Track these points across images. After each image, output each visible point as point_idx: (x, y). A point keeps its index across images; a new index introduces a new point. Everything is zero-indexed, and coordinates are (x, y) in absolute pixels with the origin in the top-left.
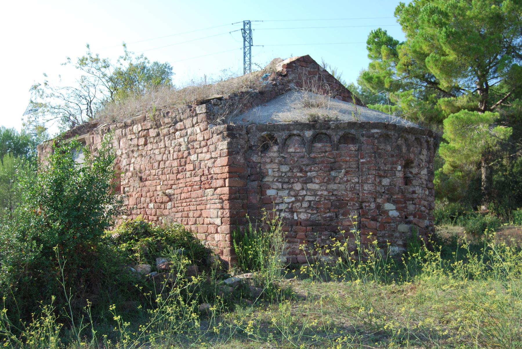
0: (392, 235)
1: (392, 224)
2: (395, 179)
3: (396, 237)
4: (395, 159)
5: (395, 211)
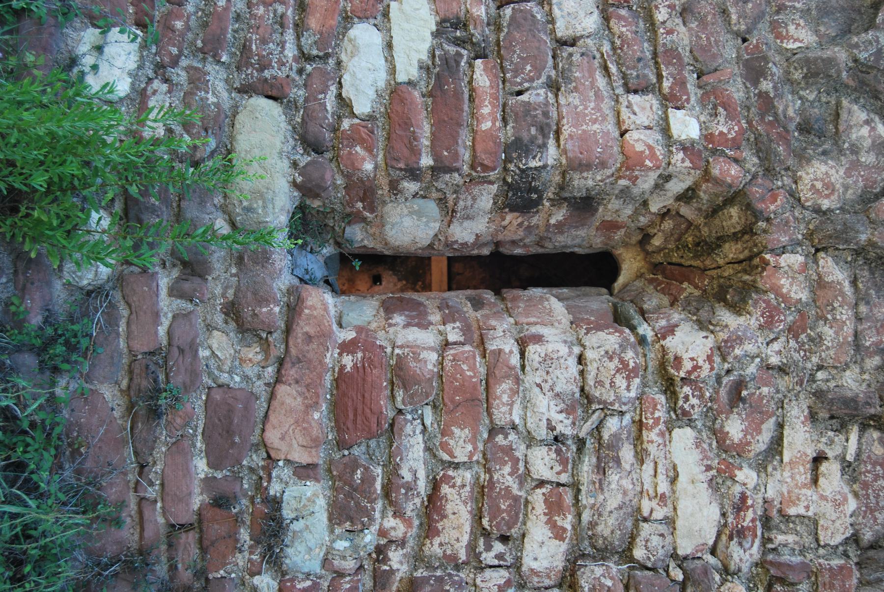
0: (210, 49)
1: (290, 36)
2: (601, 82)
3: (197, 80)
4: (737, 91)
5: (381, 78)
